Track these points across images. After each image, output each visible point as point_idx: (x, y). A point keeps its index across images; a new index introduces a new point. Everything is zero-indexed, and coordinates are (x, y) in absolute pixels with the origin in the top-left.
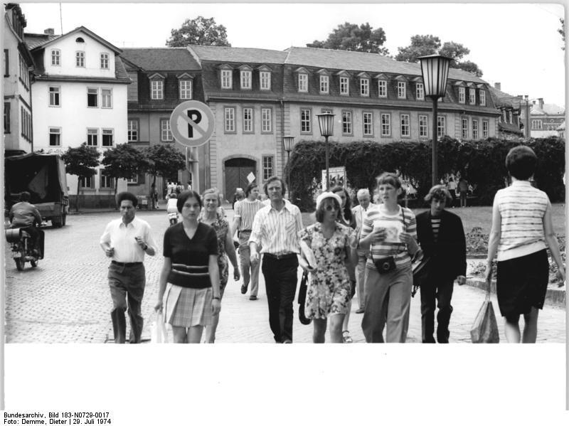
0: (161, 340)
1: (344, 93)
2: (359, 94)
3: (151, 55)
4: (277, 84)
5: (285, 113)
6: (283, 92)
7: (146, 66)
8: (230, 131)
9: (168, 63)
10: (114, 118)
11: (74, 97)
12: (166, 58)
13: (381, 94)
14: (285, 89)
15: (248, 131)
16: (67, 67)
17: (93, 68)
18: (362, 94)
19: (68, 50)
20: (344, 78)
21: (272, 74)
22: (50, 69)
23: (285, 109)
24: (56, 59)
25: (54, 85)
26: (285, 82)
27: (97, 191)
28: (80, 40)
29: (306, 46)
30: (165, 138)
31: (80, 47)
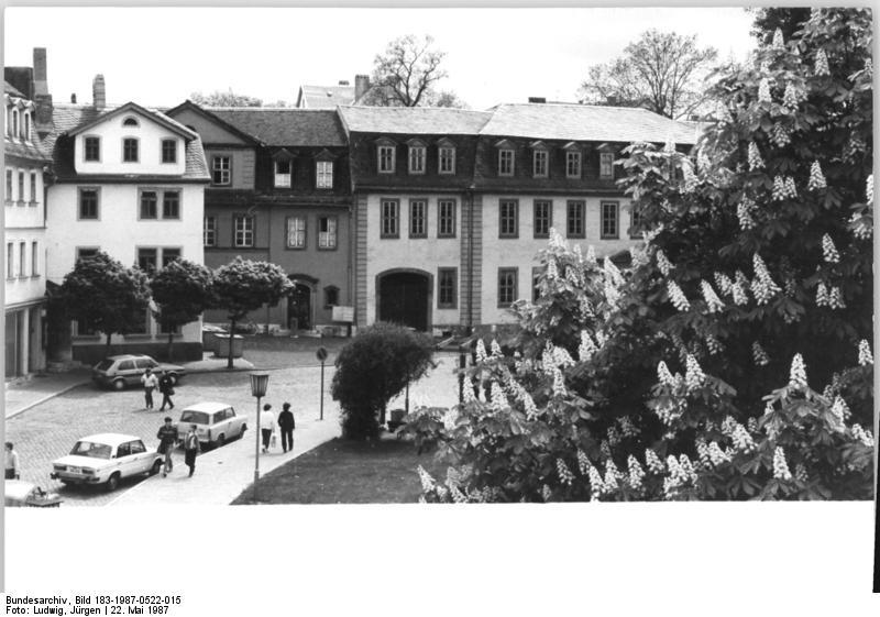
0: (153, 205)
1: (573, 176)
2: (497, 174)
3: (282, 120)
4: (466, 167)
5: (475, 208)
6: (473, 177)
7: (268, 139)
8: (389, 230)
9: (303, 134)
10: (187, 234)
11: (119, 205)
12: (302, 126)
13: (570, 172)
14: (476, 172)
15: (446, 233)
16: (111, 160)
17: (150, 162)
18: (568, 175)
19: (111, 137)
20: (573, 154)
21: (457, 149)
22: (82, 166)
23: (475, 203)
24: (93, 151)
25: (88, 187)
26: (479, 162)
27: (154, 338)
28: (130, 122)
29: (527, 101)
30: (240, 242)
31: (131, 132)
